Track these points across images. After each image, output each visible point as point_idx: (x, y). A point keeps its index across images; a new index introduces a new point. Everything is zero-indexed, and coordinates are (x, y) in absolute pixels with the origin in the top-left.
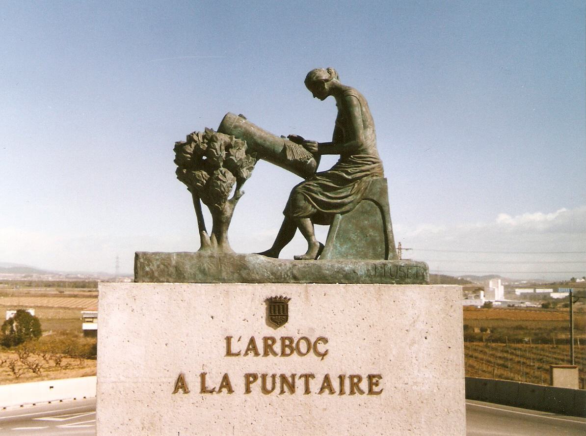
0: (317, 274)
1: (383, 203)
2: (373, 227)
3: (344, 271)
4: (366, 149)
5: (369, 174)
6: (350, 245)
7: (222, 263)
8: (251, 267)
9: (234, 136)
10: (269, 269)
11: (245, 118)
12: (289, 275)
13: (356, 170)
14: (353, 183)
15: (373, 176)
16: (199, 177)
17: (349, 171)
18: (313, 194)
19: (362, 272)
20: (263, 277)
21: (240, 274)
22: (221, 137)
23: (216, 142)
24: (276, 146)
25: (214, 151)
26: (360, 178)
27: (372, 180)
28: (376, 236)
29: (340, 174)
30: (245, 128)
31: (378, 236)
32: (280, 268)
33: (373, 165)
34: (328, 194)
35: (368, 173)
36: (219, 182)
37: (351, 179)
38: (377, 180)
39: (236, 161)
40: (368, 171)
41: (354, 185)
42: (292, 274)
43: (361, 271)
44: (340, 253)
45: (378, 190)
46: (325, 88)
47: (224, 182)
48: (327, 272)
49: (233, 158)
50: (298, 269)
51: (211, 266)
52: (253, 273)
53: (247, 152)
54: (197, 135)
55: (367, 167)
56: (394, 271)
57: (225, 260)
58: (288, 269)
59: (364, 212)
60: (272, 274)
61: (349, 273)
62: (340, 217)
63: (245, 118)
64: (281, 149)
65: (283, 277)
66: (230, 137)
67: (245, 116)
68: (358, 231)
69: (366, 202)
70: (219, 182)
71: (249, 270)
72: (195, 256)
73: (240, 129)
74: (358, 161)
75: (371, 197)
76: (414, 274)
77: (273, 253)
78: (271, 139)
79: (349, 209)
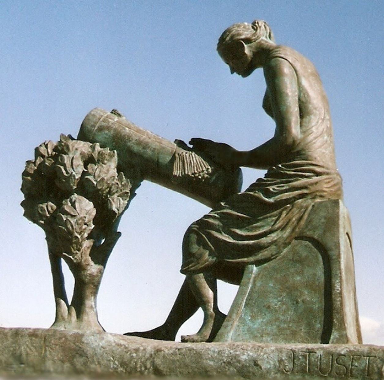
0: (194, 365)
1: (329, 242)
2: (310, 286)
3: (239, 361)
4: (303, 150)
5: (307, 194)
6: (268, 317)
7: (47, 346)
8: (90, 352)
9: (98, 144)
10: (118, 356)
11: (119, 115)
12: (148, 366)
13: (283, 186)
14: (278, 211)
15: (314, 198)
16: (41, 210)
17: (271, 190)
18: (214, 233)
19: (270, 364)
20: (106, 370)
21: (73, 364)
22: (76, 146)
23: (66, 154)
24: (161, 156)
25: (62, 168)
26: (287, 201)
27: (313, 204)
28: (314, 303)
29: (256, 194)
30: (115, 130)
31: (316, 301)
32: (134, 355)
33: (315, 179)
34: (238, 231)
35: (305, 191)
36: (64, 217)
37: (272, 203)
38: (321, 203)
39: (95, 183)
40: (305, 187)
41: (281, 214)
42: (153, 366)
43: (268, 362)
44: (249, 330)
45: (323, 220)
46: (245, 54)
47: (73, 216)
48: (211, 363)
49: (90, 178)
50: (164, 357)
51: (30, 349)
52: (93, 362)
53: (119, 169)
54: (46, 146)
55: (302, 181)
56: (327, 364)
57: (53, 342)
58: (147, 356)
59: (298, 260)
60: (123, 364)
61: (246, 366)
62: (255, 268)
63: (119, 115)
64: (169, 158)
65: (139, 369)
66: (91, 146)
67: (120, 112)
68: (284, 294)
69: (302, 243)
70: (64, 217)
71: (87, 357)
72: (10, 334)
73: (107, 132)
74: (288, 173)
75: (309, 233)
76: (363, 370)
77: (166, 332)
78: (155, 145)
79: (269, 256)
